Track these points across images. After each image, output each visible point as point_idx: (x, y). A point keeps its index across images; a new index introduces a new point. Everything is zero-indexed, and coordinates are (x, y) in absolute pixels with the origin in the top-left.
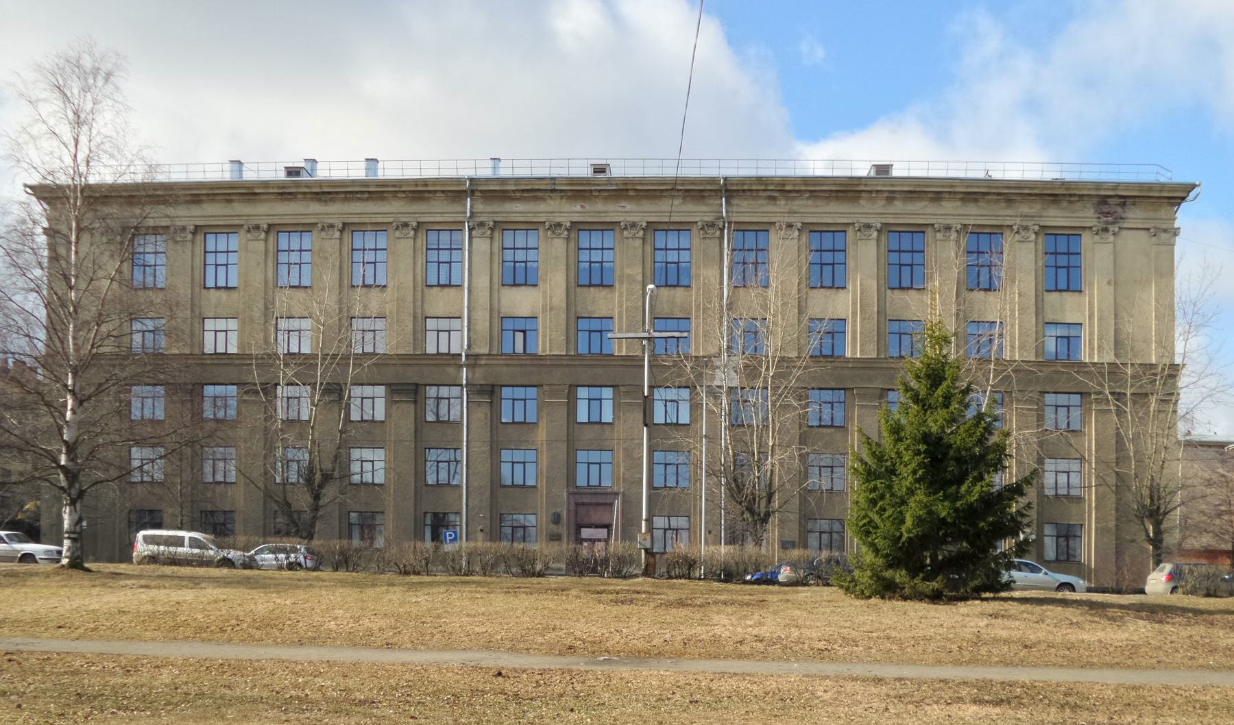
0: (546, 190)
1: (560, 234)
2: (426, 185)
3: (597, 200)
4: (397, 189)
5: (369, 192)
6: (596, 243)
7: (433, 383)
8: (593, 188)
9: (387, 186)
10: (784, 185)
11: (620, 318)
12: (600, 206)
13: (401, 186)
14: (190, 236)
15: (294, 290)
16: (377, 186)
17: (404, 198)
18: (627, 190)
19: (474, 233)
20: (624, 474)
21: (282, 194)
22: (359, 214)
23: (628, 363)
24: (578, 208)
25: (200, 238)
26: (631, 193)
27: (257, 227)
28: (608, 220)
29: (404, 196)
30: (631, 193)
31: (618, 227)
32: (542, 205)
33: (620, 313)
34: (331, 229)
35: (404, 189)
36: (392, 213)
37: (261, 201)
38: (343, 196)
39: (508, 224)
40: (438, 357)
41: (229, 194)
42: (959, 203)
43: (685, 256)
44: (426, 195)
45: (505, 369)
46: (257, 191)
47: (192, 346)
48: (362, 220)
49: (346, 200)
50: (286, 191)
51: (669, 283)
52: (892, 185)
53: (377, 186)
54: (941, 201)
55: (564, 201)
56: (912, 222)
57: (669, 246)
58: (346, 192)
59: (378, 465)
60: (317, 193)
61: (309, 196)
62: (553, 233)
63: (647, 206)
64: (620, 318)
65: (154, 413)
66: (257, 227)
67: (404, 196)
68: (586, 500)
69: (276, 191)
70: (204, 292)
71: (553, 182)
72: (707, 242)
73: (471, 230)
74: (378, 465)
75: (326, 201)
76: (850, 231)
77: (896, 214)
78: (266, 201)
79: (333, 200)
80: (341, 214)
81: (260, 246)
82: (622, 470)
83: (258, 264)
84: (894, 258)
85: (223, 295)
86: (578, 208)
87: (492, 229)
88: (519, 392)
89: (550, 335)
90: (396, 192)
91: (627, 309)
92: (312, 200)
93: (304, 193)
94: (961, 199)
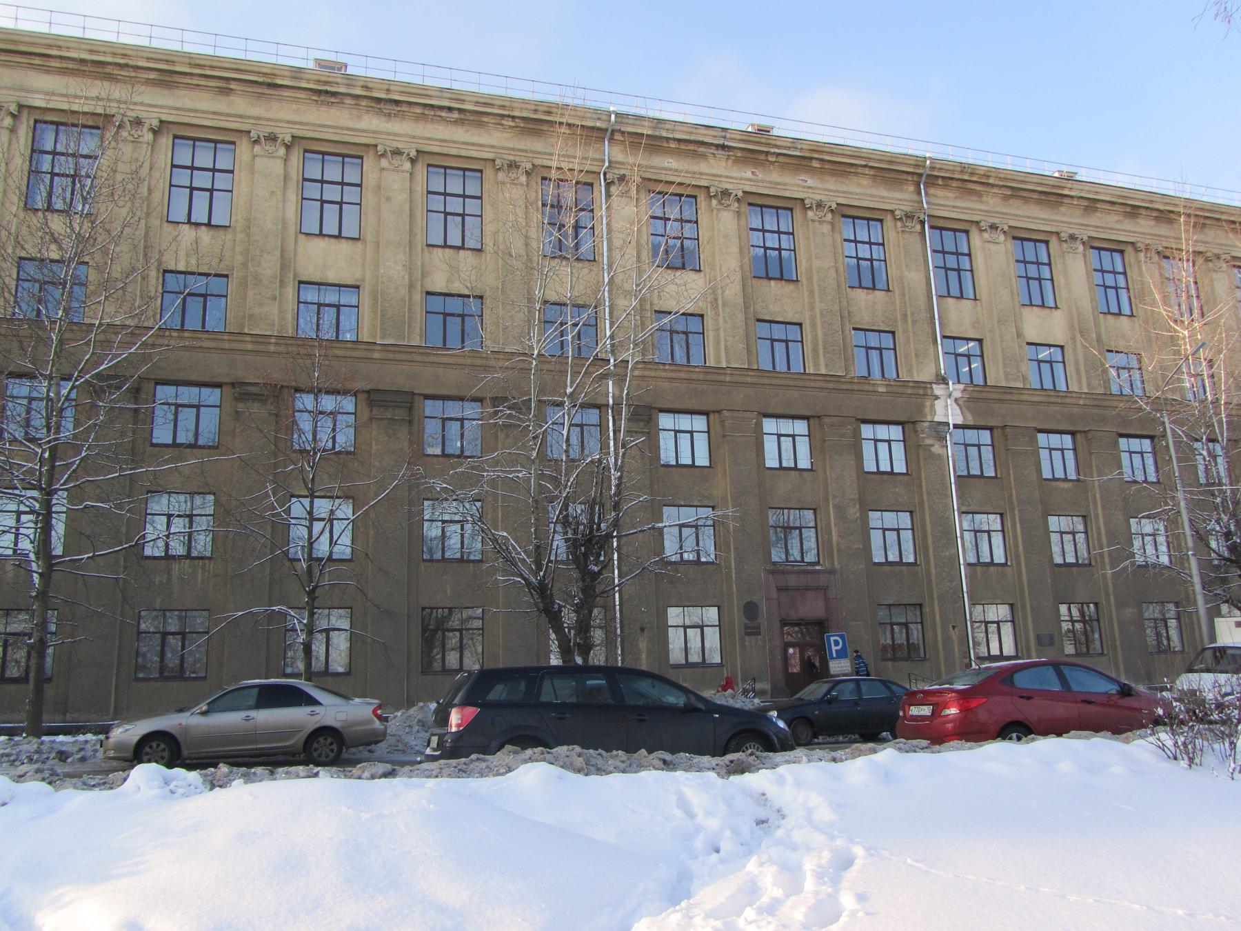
0: (712, 144)
1: (729, 205)
2: (549, 113)
3: (771, 168)
4: (506, 113)
5: (460, 110)
6: (333, 173)
7: (698, 407)
8: (772, 150)
9: (492, 105)
10: (988, 177)
11: (813, 325)
12: (775, 176)
13: (512, 109)
14: (149, 137)
15: (351, 242)
16: (149, 59)
17: (511, 127)
18: (811, 159)
19: (613, 189)
20: (838, 544)
21: (320, 92)
22: (441, 141)
23: (831, 385)
24: (749, 175)
25: (165, 141)
26: (815, 164)
27: (272, 138)
28: (788, 194)
29: (512, 124)
30: (815, 164)
31: (371, 153)
32: (702, 165)
33: (813, 319)
34: (397, 157)
35: (516, 113)
36: (493, 147)
37: (280, 99)
38: (418, 110)
39: (942, 220)
40: (804, 377)
41: (227, 79)
42: (1153, 223)
43: (877, 252)
44: (545, 128)
45: (667, 385)
46: (279, 82)
47: (1105, 388)
48: (445, 151)
49: (421, 118)
50: (329, 89)
51: (324, 232)
52: (1097, 193)
53: (149, 59)
54: (1137, 218)
55: (730, 162)
56: (1113, 237)
57: (767, 227)
58: (425, 105)
59: (202, 524)
60: (379, 100)
61: (364, 103)
62: (720, 203)
63: (832, 184)
64: (813, 325)
65: (334, 438)
66: (272, 138)
67: (512, 124)
68: (792, 581)
69: (312, 86)
70: (168, 228)
71: (723, 134)
72: (906, 236)
73: (608, 185)
74: (202, 524)
75: (389, 115)
76: (489, 173)
77: (1098, 227)
78: (188, 86)
79: (400, 116)
80: (414, 137)
81: (277, 167)
82: (835, 538)
83: (273, 193)
84: (437, 203)
85: (205, 235)
86: (749, 175)
87: (288, 147)
88: (684, 422)
89: (726, 340)
90: (503, 116)
91: (822, 314)
92: (369, 109)
93: (358, 97)
94: (1156, 218)
